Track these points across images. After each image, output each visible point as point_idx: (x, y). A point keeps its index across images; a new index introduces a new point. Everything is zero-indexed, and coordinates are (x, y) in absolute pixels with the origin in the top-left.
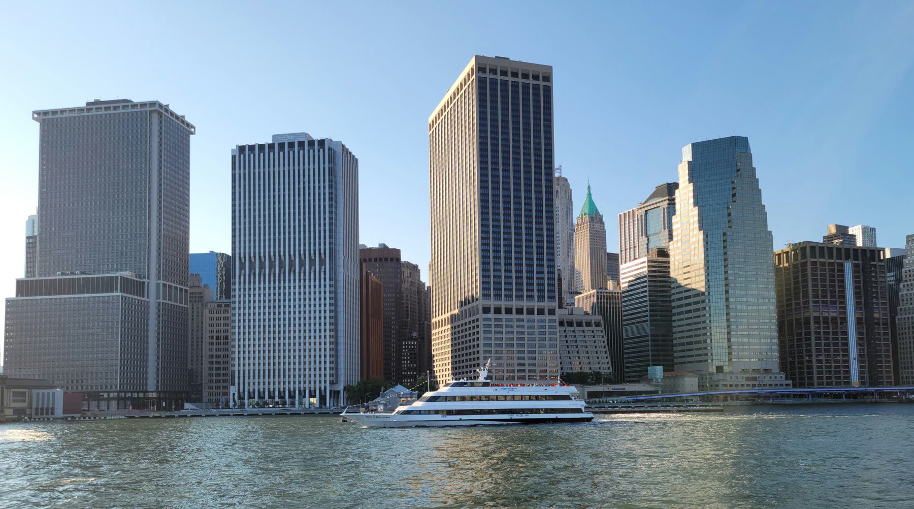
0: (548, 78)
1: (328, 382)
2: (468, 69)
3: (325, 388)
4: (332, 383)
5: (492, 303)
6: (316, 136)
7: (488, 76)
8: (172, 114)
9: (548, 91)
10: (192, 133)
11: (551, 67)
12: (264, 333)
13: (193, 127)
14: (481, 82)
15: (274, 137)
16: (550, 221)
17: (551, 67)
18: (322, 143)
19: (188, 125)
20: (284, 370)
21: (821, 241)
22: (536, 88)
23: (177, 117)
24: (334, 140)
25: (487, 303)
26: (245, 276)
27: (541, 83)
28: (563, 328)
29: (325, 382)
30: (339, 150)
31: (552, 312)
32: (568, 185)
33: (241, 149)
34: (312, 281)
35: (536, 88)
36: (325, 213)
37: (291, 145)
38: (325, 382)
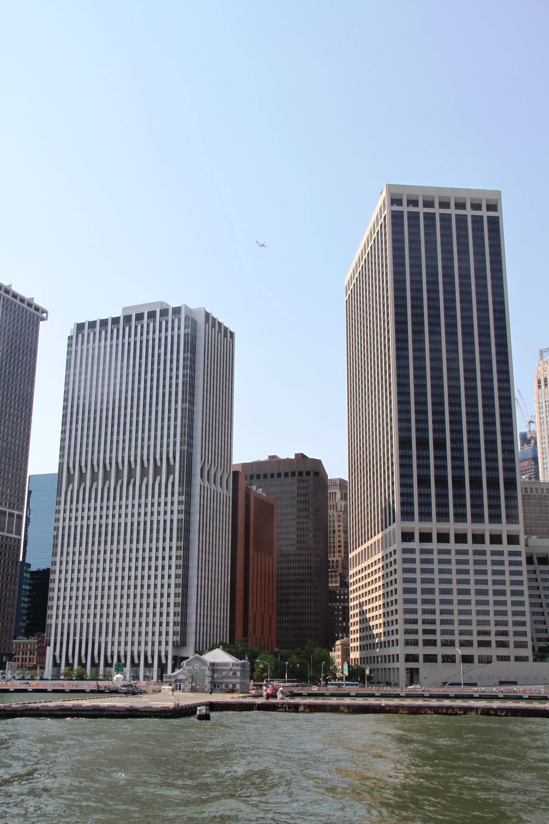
0: (493, 207)
1: (171, 644)
2: (380, 202)
3: (166, 652)
4: (175, 645)
5: (416, 526)
6: (174, 304)
7: (405, 209)
8: (15, 296)
9: (495, 224)
10: (43, 319)
11: (499, 193)
12: (124, 560)
13: (44, 311)
14: (396, 217)
15: (124, 309)
16: (505, 385)
17: (499, 193)
18: (177, 311)
19: (37, 309)
20: (114, 624)
21: (293, 457)
22: (477, 220)
23: (22, 300)
24: (192, 307)
25: (408, 526)
26: (72, 492)
27: (484, 213)
28: (532, 567)
29: (167, 643)
30: (201, 320)
31: (513, 539)
32: (449, 655)
33: (80, 327)
34: (143, 497)
35: (477, 220)
36: (176, 402)
37: (140, 317)
38: (167, 643)
